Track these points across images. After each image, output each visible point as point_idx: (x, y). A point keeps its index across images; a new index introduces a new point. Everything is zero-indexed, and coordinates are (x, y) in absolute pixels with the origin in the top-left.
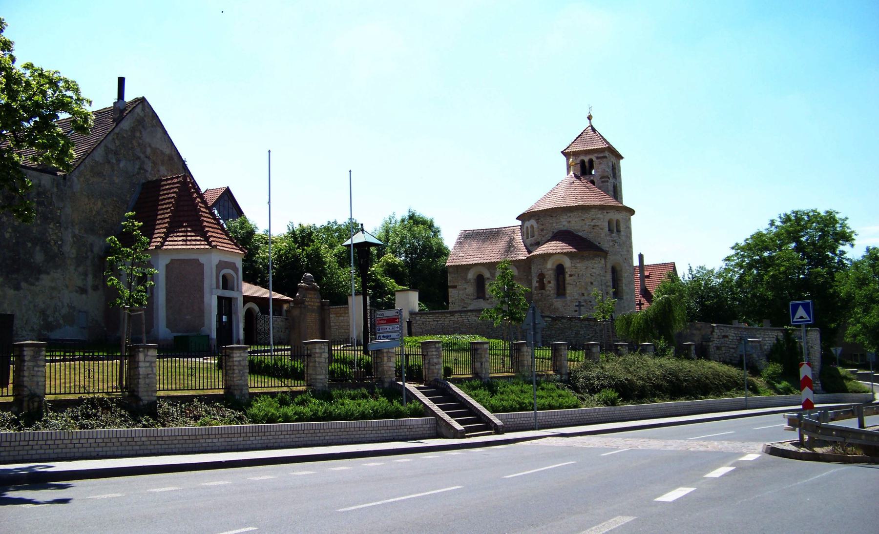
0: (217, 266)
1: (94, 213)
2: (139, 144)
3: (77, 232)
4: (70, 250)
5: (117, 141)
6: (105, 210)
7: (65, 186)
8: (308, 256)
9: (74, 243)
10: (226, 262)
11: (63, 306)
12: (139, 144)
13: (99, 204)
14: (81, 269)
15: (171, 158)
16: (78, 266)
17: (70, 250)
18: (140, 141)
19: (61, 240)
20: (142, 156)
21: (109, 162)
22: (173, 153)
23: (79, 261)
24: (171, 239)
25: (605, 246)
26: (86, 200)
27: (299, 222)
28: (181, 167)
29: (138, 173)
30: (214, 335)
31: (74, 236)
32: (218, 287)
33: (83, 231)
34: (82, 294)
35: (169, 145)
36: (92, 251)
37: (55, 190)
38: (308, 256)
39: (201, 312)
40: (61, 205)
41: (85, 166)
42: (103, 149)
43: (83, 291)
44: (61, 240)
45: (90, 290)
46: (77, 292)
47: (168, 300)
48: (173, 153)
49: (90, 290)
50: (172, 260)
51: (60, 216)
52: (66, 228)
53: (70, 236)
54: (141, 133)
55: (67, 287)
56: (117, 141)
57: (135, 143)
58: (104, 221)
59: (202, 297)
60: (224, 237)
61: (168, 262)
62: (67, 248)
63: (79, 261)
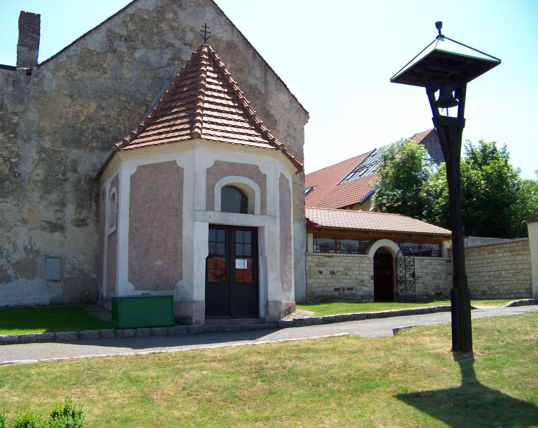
0: (208, 171)
1: (82, 118)
2: (172, 29)
3: (47, 144)
4: (31, 168)
5: (130, 25)
6: (103, 113)
7: (28, 83)
8: (488, 177)
9: (41, 160)
10: (232, 165)
11: (15, 249)
12: (172, 29)
13: (93, 106)
14: (53, 196)
15: (231, 46)
16: (47, 191)
17: (31, 168)
18: (176, 24)
19: (18, 156)
20: (177, 43)
21: (115, 51)
22: (236, 39)
23: (49, 185)
24: (144, 134)
25: (395, 401)
26: (68, 101)
27: (480, 139)
28: (250, 57)
29: (169, 65)
30: (199, 293)
31: (42, 150)
32: (210, 207)
33: (59, 144)
34: (52, 231)
35: (229, 29)
36: (75, 171)
37: (11, 89)
38: (488, 177)
39: (176, 255)
40: (19, 108)
41: (68, 57)
42: (104, 34)
43: (56, 227)
44: (18, 156)
45: (70, 227)
46: (44, 229)
47: (132, 235)
48: (236, 39)
49: (70, 227)
50: (139, 167)
51: (17, 125)
52: (27, 140)
53: (34, 151)
54: (175, 13)
55: (25, 222)
56: (130, 25)
57: (164, 26)
58: (102, 129)
59: (180, 226)
60: (254, 132)
61: (133, 171)
62: (26, 168)
63: (49, 185)
